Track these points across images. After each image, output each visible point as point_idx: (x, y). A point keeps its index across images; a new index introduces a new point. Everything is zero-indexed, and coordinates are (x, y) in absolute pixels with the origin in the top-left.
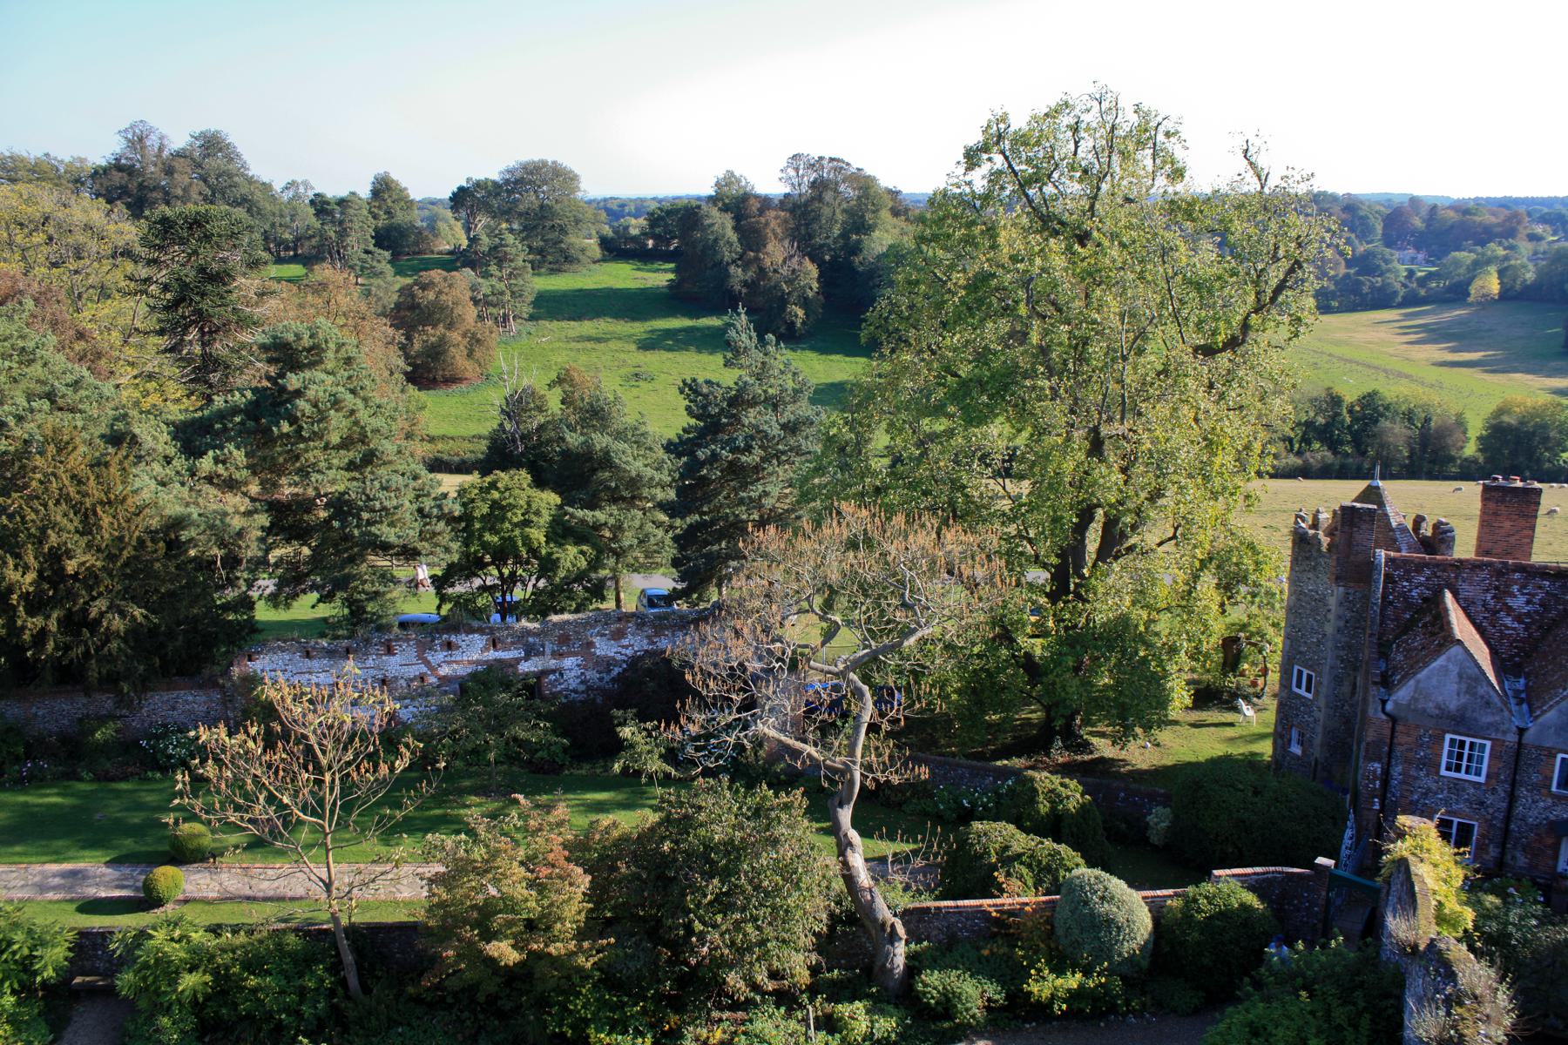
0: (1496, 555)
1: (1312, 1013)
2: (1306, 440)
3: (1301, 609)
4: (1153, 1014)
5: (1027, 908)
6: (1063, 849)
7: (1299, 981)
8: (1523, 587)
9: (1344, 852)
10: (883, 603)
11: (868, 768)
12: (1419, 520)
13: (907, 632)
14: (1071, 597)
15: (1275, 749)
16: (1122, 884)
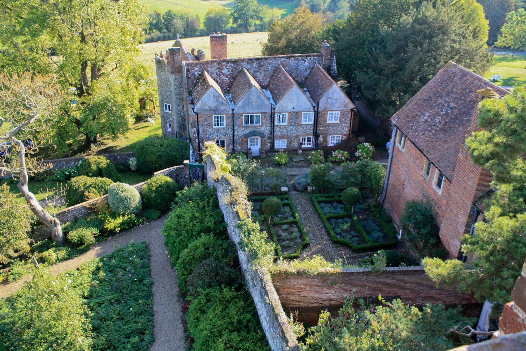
0: (217, 58)
1: (194, 206)
2: (151, 29)
3: (162, 84)
4: (147, 222)
5: (99, 201)
6: (105, 179)
7: (188, 198)
8: (226, 66)
9: (191, 157)
10: (17, 109)
11: (30, 169)
12: (193, 51)
13: (31, 117)
14: (86, 94)
15: (163, 131)
16: (127, 185)
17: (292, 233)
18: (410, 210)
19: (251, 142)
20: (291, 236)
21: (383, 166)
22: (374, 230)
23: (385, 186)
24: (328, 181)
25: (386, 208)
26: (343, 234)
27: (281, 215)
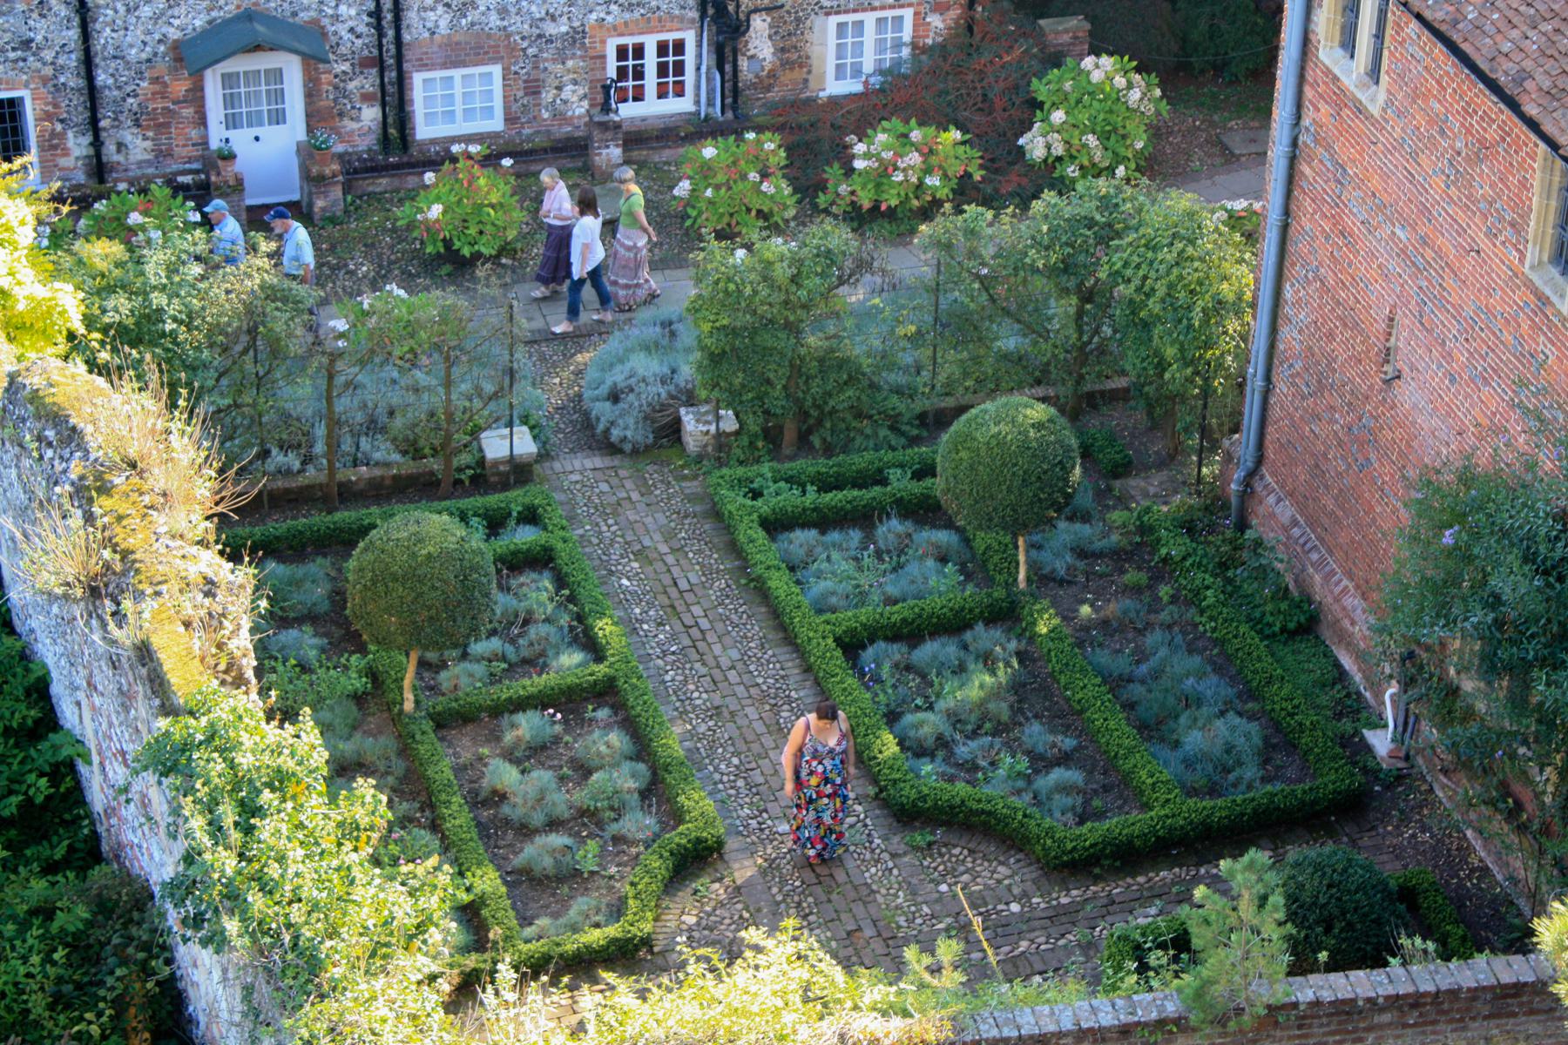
17: (584, 771)
18: (1448, 538)
19: (230, 101)
20: (581, 796)
21: (1234, 220)
22: (1192, 701)
23: (1256, 370)
24: (831, 363)
25: (1270, 537)
26: (964, 750)
27: (495, 644)
